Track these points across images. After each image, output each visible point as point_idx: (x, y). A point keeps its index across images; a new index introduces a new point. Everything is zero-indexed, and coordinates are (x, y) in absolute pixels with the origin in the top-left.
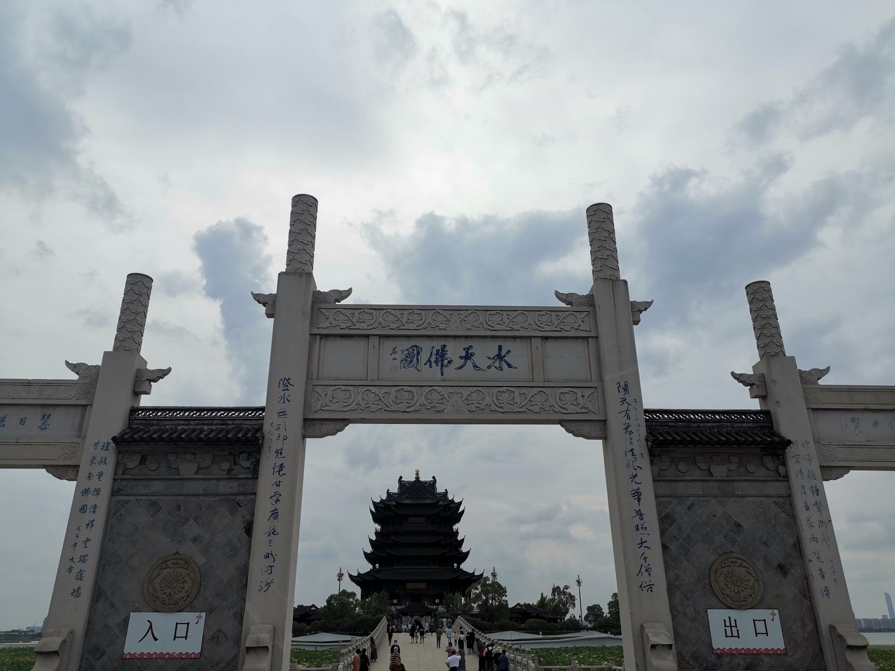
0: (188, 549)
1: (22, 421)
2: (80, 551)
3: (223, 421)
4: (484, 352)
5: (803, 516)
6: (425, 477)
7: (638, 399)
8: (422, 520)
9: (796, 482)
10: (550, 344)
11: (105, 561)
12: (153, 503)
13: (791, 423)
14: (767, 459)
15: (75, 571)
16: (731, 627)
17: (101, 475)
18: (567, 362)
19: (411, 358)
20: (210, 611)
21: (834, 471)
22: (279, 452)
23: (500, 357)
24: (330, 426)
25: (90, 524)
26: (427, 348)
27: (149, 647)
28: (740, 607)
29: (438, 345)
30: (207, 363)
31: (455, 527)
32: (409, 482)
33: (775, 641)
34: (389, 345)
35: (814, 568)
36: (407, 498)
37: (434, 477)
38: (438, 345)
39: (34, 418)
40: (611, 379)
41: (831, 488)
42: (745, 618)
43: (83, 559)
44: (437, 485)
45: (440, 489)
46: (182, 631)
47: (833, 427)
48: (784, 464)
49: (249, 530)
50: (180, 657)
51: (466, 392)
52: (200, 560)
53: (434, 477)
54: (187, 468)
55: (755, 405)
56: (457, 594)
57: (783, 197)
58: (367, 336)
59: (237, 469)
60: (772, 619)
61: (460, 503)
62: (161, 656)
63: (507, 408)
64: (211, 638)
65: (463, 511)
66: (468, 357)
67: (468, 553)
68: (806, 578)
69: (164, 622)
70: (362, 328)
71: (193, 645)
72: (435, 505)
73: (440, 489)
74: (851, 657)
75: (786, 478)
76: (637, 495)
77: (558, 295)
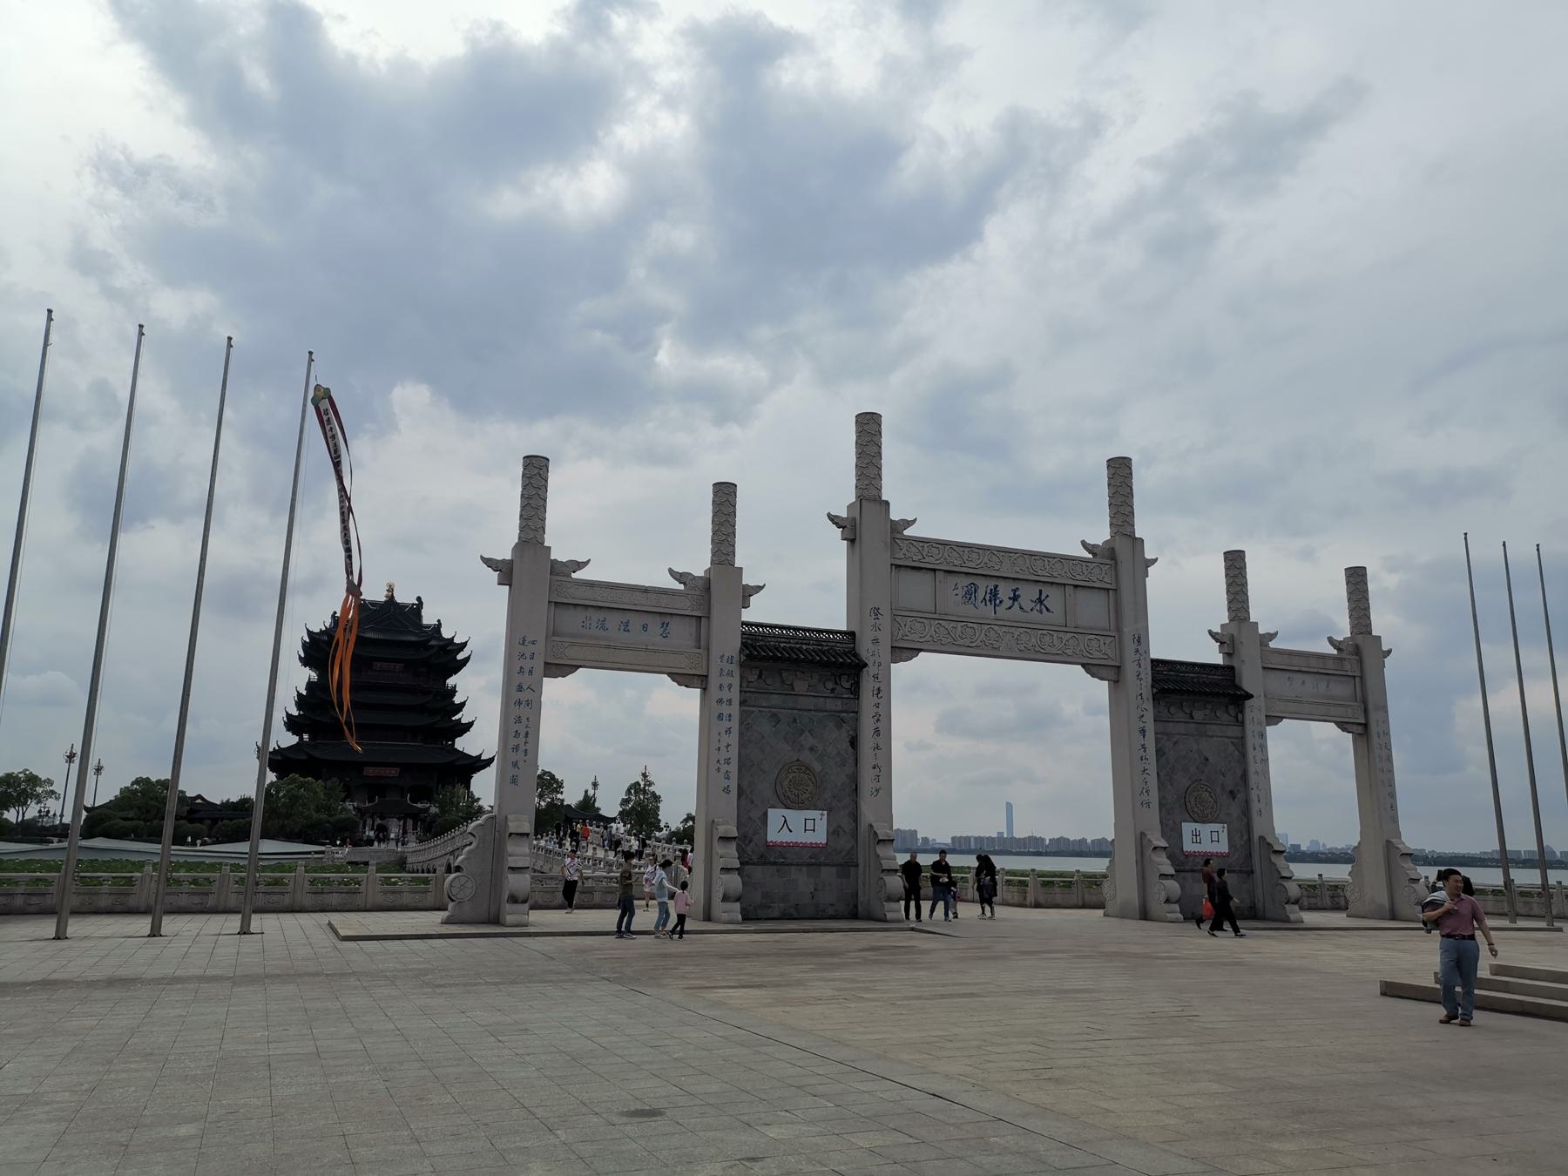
0: (806, 757)
1: (645, 627)
2: (723, 755)
3: (819, 642)
4: (1028, 594)
5: (1251, 754)
6: (404, 597)
7: (1147, 652)
8: (399, 666)
9: (1250, 728)
10: (1081, 594)
11: (745, 765)
12: (774, 715)
13: (1250, 679)
14: (1231, 707)
15: (723, 771)
16: (1196, 834)
17: (730, 686)
18: (1091, 609)
19: (971, 593)
20: (830, 811)
21: (1273, 719)
22: (876, 677)
23: (1040, 601)
24: (905, 655)
25: (728, 731)
26: (984, 586)
27: (785, 837)
28: (1204, 822)
29: (991, 584)
30: (801, 585)
31: (451, 682)
32: (373, 603)
33: (1223, 847)
34: (952, 580)
35: (1254, 795)
36: (373, 630)
37: (419, 599)
38: (991, 584)
39: (655, 625)
40: (1128, 630)
41: (1271, 731)
42: (1206, 829)
43: (728, 761)
44: (424, 612)
45: (428, 618)
46: (810, 825)
47: (1277, 683)
48: (1242, 712)
49: (854, 742)
50: (812, 846)
51: (1017, 632)
52: (817, 767)
53: (419, 599)
54: (801, 686)
55: (1218, 659)
56: (458, 786)
57: (951, 126)
58: (934, 570)
59: (839, 689)
60: (1221, 830)
61: (464, 645)
62: (796, 845)
63: (1048, 649)
64: (833, 832)
65: (467, 660)
66: (1015, 598)
67: (471, 724)
68: (1247, 802)
69: (796, 817)
70: (931, 562)
71: (820, 837)
72: (423, 645)
73: (428, 618)
74: (1274, 858)
75: (1242, 724)
76: (1143, 732)
77: (1084, 544)
